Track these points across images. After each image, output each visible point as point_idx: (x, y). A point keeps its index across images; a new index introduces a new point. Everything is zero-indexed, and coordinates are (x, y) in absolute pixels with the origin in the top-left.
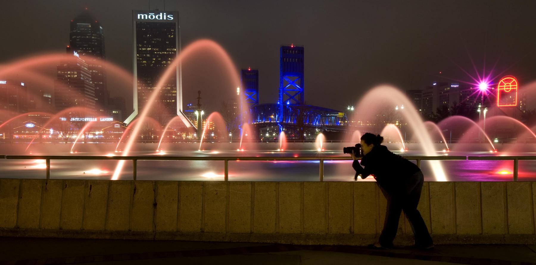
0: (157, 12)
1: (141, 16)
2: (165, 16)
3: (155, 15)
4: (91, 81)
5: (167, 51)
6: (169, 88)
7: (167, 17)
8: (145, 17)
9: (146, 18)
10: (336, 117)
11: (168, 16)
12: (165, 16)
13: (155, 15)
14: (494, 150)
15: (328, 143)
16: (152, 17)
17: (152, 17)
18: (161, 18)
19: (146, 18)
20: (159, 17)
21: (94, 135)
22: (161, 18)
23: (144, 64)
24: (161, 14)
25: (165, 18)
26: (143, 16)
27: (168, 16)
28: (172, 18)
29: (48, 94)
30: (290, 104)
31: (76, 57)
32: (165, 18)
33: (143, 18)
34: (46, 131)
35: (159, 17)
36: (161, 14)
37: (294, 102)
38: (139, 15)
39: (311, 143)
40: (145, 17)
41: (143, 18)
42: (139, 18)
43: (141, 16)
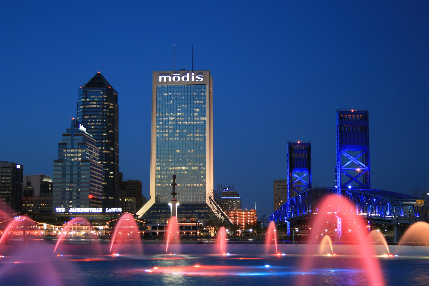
0: (183, 71)
1: (163, 78)
2: (193, 77)
3: (181, 76)
4: (99, 161)
5: (194, 121)
6: (197, 168)
7: (195, 78)
8: (167, 79)
9: (170, 80)
10: (413, 205)
11: (197, 77)
12: (193, 77)
13: (181, 76)
14: (388, 254)
15: (186, 245)
16: (176, 79)
17: (176, 79)
18: (188, 80)
19: (170, 80)
20: (185, 79)
21: (97, 230)
22: (188, 80)
23: (165, 137)
24: (188, 74)
25: (193, 80)
26: (165, 77)
27: (197, 77)
28: (202, 79)
29: (49, 178)
30: (352, 188)
31: (83, 132)
32: (193, 80)
33: (165, 80)
34: (38, 225)
35: (185, 79)
36: (188, 74)
37: (357, 185)
38: (160, 77)
39: (156, 245)
40: (167, 79)
41: (165, 80)
42: (160, 80)
43: (163, 78)
